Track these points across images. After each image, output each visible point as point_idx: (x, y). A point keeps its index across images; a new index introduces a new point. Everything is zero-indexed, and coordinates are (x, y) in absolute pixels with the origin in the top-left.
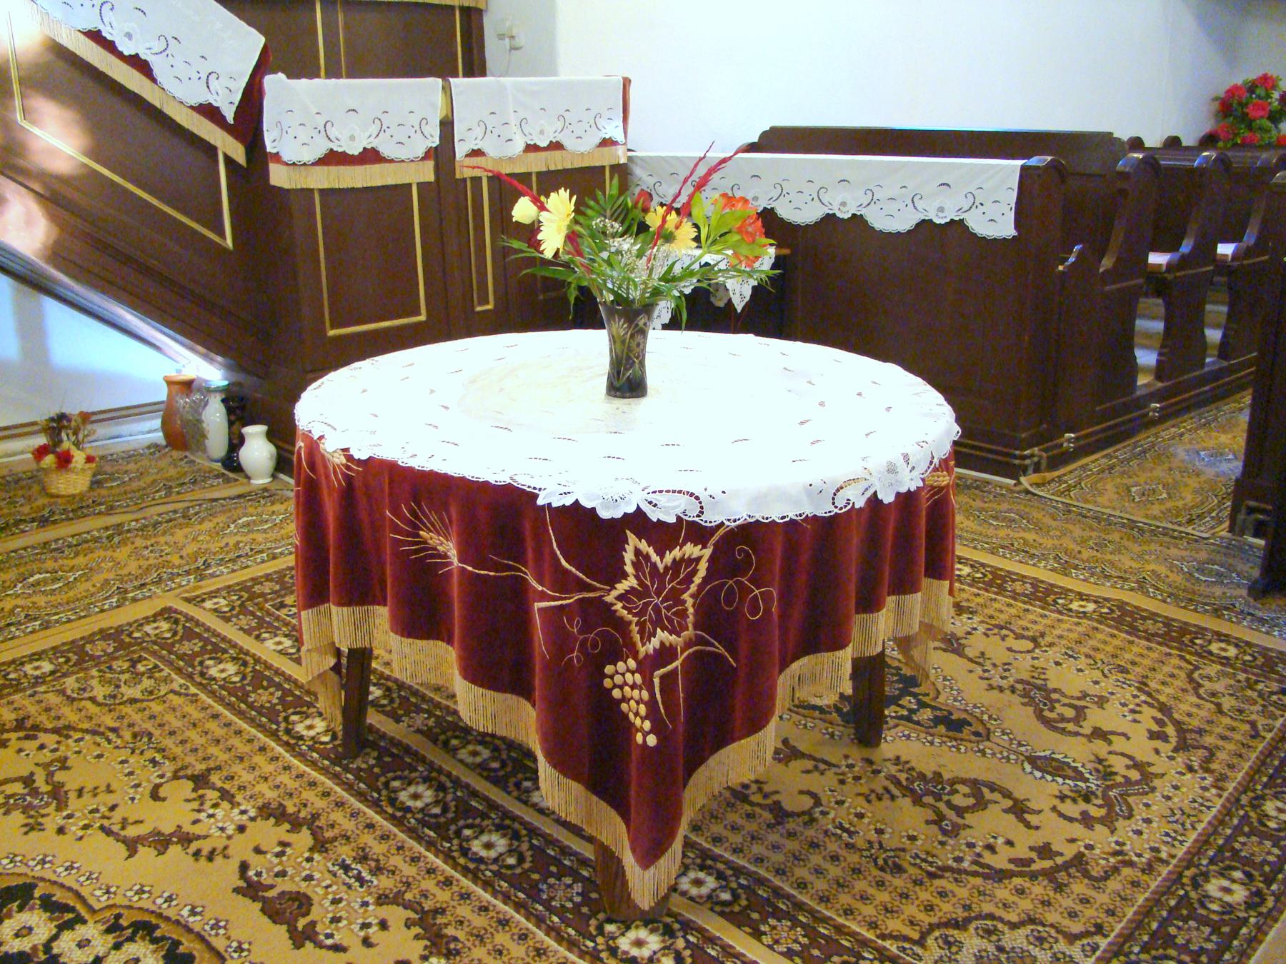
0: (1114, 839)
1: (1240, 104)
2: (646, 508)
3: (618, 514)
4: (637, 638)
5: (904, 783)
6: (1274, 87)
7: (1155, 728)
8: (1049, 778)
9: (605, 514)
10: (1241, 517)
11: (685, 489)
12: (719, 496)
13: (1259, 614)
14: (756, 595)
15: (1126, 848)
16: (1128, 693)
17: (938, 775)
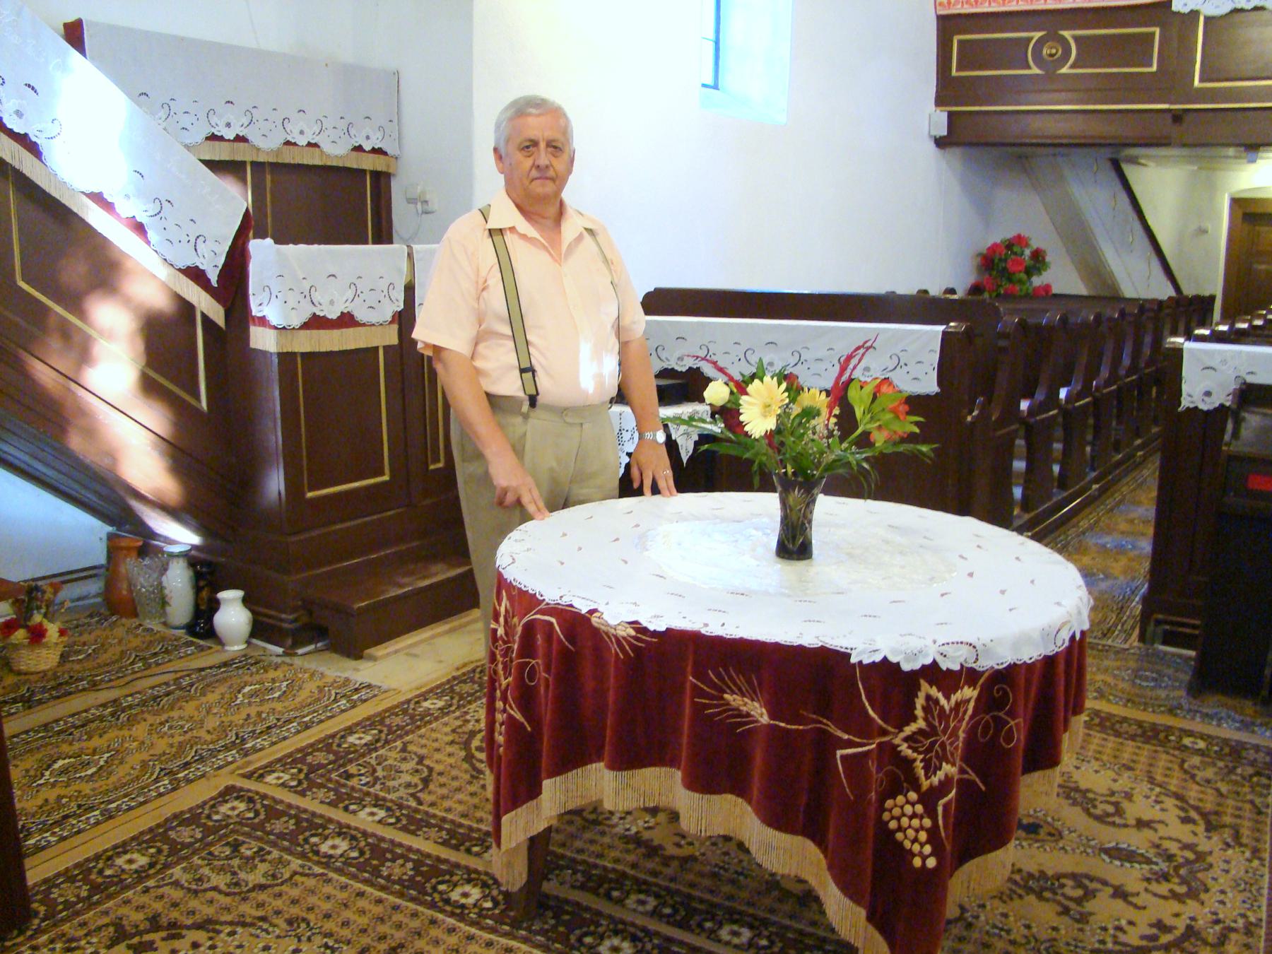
0: (1207, 910)
1: (1000, 260)
2: (940, 660)
3: (917, 666)
4: (921, 773)
5: (1022, 883)
6: (1027, 245)
7: (1182, 814)
8: (1128, 865)
9: (906, 667)
10: (1151, 628)
11: (964, 640)
12: (990, 645)
13: (1205, 711)
14: (1011, 727)
15: (1221, 916)
16: (1145, 787)
17: (1042, 873)
